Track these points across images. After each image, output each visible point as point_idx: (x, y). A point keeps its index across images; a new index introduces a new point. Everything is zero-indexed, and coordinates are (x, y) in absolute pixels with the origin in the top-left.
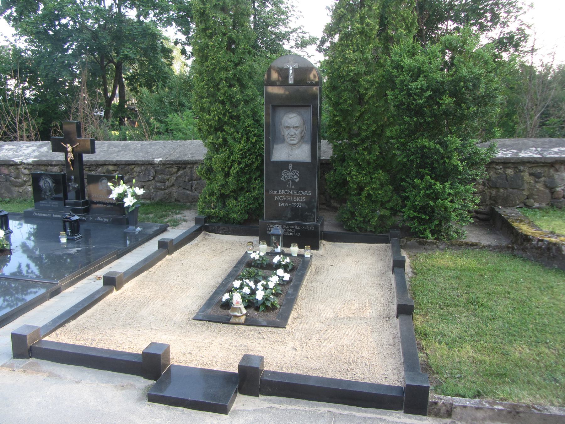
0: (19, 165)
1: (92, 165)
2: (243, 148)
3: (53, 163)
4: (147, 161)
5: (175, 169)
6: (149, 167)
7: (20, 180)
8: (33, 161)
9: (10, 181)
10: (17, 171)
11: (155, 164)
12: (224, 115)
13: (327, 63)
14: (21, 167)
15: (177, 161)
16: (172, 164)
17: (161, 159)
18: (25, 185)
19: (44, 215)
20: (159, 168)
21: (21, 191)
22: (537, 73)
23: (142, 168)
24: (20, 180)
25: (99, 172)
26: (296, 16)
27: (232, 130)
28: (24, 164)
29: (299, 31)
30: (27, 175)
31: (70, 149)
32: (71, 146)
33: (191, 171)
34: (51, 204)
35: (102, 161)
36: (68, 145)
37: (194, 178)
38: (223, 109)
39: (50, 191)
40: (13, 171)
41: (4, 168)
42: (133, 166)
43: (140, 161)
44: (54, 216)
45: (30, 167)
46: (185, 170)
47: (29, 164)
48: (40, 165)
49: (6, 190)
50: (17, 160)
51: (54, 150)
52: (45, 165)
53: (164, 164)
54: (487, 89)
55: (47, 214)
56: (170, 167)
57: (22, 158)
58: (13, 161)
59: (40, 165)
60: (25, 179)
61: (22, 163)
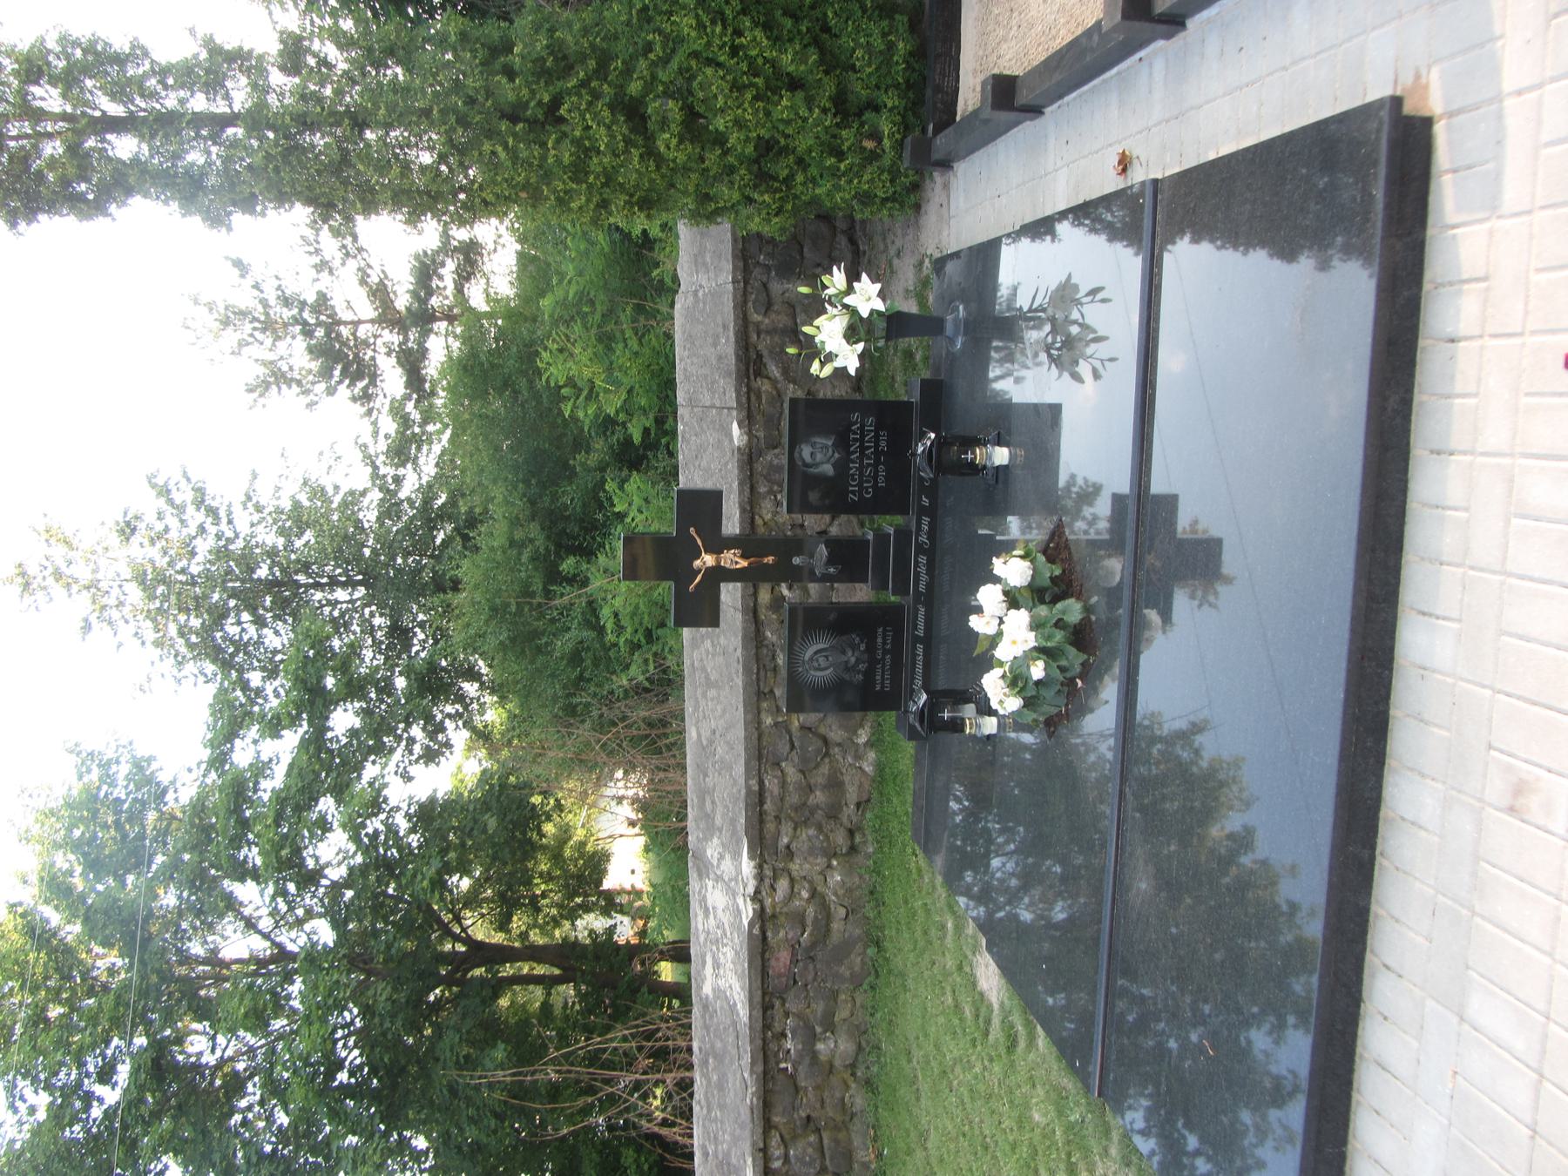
0: (763, 909)
1: (757, 654)
2: (692, 14)
3: (756, 788)
4: (741, 468)
5: (765, 386)
6: (758, 467)
7: (811, 912)
8: (751, 857)
9: (814, 945)
10: (782, 919)
11: (749, 444)
12: (596, 95)
13: (465, 368)
14: (768, 902)
15: (738, 371)
16: (749, 389)
17: (735, 425)
18: (823, 897)
19: (919, 668)
20: (761, 434)
21: (842, 912)
22: (512, 1021)
23: (762, 490)
24: (811, 912)
25: (779, 638)
26: (332, 462)
27: (642, 64)
28: (757, 891)
29: (372, 451)
30: (792, 888)
31: (709, 560)
32: (698, 556)
33: (768, 332)
34: (885, 652)
35: (745, 621)
36: (697, 563)
37: (790, 323)
38: (580, 96)
39: (844, 652)
40: (782, 934)
41: (773, 962)
42: (759, 521)
43: (741, 492)
44: (921, 633)
45: (768, 872)
46: (765, 353)
47: (760, 877)
48: (761, 838)
49: (841, 962)
50: (748, 911)
51: (714, 622)
52: (761, 822)
53: (750, 417)
54: (543, 145)
55: (915, 655)
56: (759, 397)
57: (740, 901)
58: (751, 924)
59: (761, 838)
60: (805, 894)
61: (756, 897)
